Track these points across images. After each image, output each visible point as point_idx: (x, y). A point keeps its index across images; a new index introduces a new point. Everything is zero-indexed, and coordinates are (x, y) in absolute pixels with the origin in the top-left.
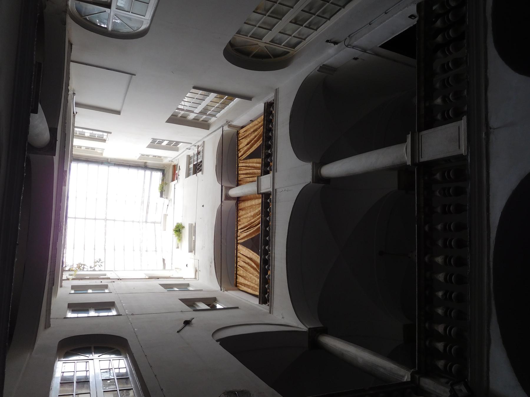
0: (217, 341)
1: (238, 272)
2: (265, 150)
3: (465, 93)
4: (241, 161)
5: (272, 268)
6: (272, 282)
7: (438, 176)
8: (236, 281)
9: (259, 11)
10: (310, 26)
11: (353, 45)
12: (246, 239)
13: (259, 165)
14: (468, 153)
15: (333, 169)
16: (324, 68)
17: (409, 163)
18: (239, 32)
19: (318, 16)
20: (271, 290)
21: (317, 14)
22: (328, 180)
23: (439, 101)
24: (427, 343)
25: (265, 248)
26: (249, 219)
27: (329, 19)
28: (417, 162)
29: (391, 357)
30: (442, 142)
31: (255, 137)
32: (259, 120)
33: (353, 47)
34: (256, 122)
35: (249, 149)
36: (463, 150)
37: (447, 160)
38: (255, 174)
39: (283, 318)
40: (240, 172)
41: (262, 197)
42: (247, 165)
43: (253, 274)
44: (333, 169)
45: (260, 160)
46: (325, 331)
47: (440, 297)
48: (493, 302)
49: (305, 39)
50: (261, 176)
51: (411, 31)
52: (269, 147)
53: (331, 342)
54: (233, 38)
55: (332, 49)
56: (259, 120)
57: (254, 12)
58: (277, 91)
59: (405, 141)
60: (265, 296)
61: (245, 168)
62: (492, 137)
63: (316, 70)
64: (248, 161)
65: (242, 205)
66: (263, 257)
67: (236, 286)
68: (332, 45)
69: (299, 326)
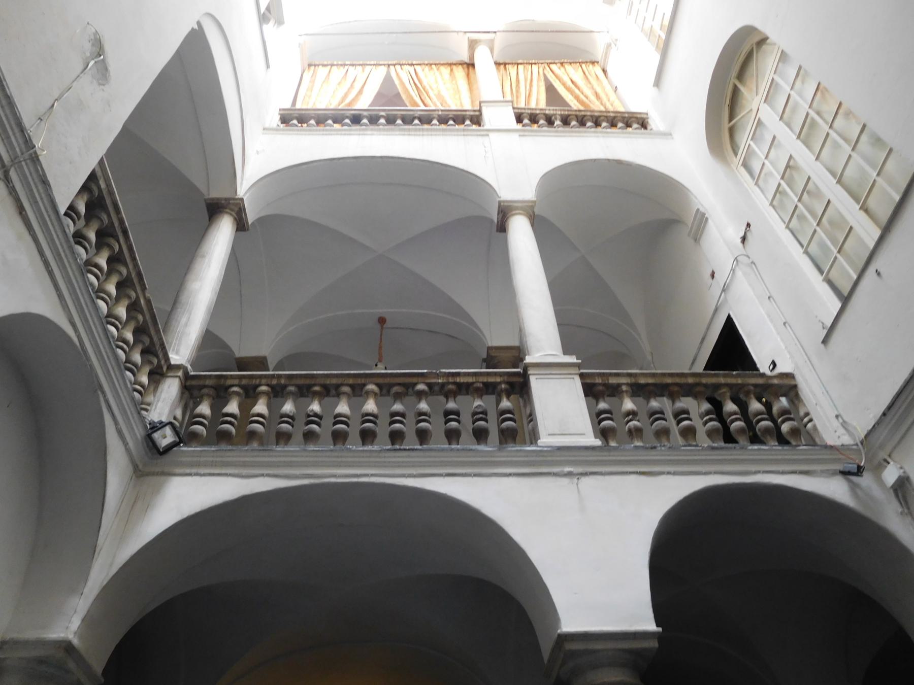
0: (199, 23)
1: (334, 68)
2: (561, 115)
5: (345, 130)
7: (505, 404)
12: (397, 82)
15: (521, 234)
16: (701, 220)
17: (528, 359)
19: (796, 206)
21: (800, 205)
22: (502, 227)
23: (628, 404)
24: (235, 389)
25: (382, 116)
30: (561, 409)
31: (587, 97)
33: (733, 270)
35: (564, 84)
36: (545, 440)
37: (531, 417)
38: (517, 97)
39: (258, 152)
41: (475, 111)
44: (521, 234)
45: (543, 104)
46: (241, 225)
47: (311, 408)
48: (306, 482)
49: (756, 184)
50: (514, 108)
52: (566, 121)
53: (223, 234)
58: (667, 135)
59: (566, 352)
62: (565, 481)
65: (460, 72)
66: (365, 113)
67: (310, 65)
68: (742, 234)
69: (244, 182)
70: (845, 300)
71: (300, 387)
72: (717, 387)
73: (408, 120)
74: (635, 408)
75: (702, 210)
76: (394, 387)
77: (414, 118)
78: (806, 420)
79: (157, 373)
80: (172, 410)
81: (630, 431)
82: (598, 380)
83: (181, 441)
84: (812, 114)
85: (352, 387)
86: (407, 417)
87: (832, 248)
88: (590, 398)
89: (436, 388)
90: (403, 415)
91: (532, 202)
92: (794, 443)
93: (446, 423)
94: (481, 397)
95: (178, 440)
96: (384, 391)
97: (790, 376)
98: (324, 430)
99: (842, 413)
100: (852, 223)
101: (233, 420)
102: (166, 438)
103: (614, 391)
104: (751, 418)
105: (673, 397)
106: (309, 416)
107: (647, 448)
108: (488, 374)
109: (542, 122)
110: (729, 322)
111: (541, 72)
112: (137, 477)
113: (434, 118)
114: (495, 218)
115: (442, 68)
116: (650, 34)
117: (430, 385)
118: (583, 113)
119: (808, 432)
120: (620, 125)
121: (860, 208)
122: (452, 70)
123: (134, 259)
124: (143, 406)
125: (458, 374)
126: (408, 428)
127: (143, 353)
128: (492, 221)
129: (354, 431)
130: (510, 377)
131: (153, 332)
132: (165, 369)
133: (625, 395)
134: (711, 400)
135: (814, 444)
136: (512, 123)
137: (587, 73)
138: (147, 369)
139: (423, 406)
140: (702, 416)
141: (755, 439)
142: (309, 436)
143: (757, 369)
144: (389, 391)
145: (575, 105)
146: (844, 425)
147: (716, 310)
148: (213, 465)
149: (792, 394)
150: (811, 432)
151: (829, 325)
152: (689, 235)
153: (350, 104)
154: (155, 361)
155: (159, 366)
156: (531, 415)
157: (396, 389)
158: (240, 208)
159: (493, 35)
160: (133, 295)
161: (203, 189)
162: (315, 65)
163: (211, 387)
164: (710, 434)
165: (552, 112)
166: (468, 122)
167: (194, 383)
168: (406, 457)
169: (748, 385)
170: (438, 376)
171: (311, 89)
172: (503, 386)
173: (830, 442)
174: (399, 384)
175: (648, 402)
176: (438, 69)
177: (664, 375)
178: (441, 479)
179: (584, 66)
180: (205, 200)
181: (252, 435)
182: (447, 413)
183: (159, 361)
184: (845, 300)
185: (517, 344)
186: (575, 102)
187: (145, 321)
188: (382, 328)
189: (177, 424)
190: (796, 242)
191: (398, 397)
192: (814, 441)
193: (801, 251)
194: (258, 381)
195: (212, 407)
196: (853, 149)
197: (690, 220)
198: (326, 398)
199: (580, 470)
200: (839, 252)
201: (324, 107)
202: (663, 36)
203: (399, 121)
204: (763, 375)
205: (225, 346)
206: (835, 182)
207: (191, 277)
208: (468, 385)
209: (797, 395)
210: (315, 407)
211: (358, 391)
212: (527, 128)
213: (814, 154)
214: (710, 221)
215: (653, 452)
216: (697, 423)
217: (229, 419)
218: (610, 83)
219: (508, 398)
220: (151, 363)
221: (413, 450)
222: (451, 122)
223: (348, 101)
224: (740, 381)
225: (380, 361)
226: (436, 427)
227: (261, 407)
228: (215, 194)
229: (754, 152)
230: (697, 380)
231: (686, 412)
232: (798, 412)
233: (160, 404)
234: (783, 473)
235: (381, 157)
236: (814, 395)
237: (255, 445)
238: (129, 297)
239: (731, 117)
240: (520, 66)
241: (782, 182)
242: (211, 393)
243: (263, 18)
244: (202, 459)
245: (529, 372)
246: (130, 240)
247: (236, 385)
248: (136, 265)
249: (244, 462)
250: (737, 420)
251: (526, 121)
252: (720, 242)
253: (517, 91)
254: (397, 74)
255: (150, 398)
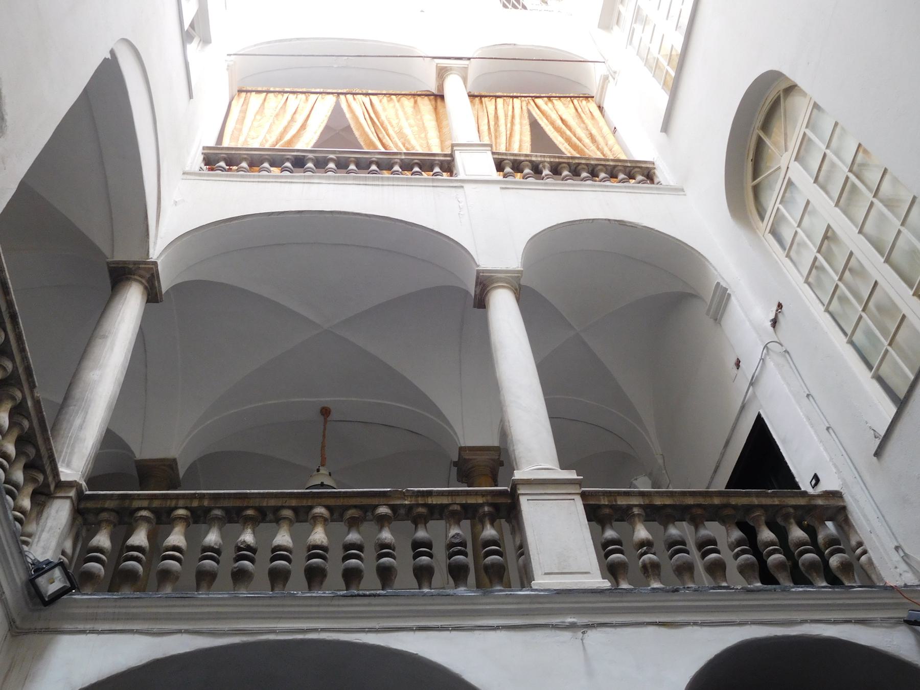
0: (112, 52)
1: (271, 95)
2: (550, 163)
3: (656, 585)
4: (524, 104)
5: (286, 177)
6: (254, 177)
7: (489, 532)
8: (251, 91)
9: (860, 155)
10: (817, 268)
11: (768, 360)
12: (348, 115)
13: (515, 150)
14: (536, 590)
15: (504, 310)
16: (723, 296)
17: (518, 475)
18: (816, 106)
19: (837, 286)
20: (237, 176)
21: (840, 284)
22: (481, 302)
23: (642, 533)
24: (144, 513)
25: (332, 160)
26: (394, 122)
27: (827, 310)
28: (519, 492)
29: (110, 439)
30: (559, 540)
31: (580, 140)
32: (616, 148)
33: (763, 360)
34: (611, 140)
35: (552, 123)
36: (541, 581)
37: (522, 550)
38: (496, 138)
39: (176, 203)
40: (500, 101)
41: (445, 155)
42: (517, 120)
43: (269, 132)
44: (504, 310)
45: (527, 150)
46: (153, 295)
47: (242, 538)
48: (236, 640)
49: (788, 256)
50: (493, 153)
51: (787, 479)
52: (556, 170)
53: (130, 307)
54: (804, 94)
55: (764, 316)
56: (616, 148)
57: (860, 145)
58: (678, 190)
59: (564, 466)
60: (219, 160)
61: (510, 113)
62: (566, 635)
63: (720, 280)
64: (526, 122)
65: (426, 105)
66: (311, 155)
67: (240, 91)
68: (772, 316)
69: (159, 241)
70: (901, 403)
71: (226, 510)
72: (749, 509)
73: (363, 165)
74: (650, 537)
75: (723, 284)
76: (349, 510)
77: (371, 163)
78: (859, 551)
79: (42, 493)
80: (60, 543)
81: (644, 567)
82: (604, 501)
83: (73, 587)
84: (852, 177)
85: (295, 510)
86: (365, 549)
87: (882, 339)
88: (594, 523)
89: (402, 511)
90: (360, 548)
91: (518, 272)
92: (847, 584)
93: (415, 557)
94: (458, 523)
95: (68, 585)
96: (336, 516)
97: (836, 495)
98: (259, 568)
99: (903, 544)
100: (905, 310)
101: (140, 555)
102: (53, 583)
103: (623, 515)
104: (792, 549)
105: (697, 523)
106: (239, 549)
107: (668, 591)
108: (468, 493)
109: (527, 171)
110: (760, 422)
111: (524, 108)
112: (13, 636)
113: (396, 163)
114: (472, 289)
115: (404, 99)
116: (655, 68)
117: (393, 508)
118: (577, 161)
119: (862, 567)
120: (621, 176)
121: (914, 295)
122: (416, 102)
123: (22, 350)
124: (23, 538)
125: (430, 493)
126: (367, 564)
127: (26, 468)
128: (467, 293)
129: (297, 569)
130: (488, 492)
131: (40, 441)
132: (52, 487)
133: (637, 519)
134: (743, 526)
135: (873, 586)
136: (491, 171)
137: (580, 110)
138: (29, 489)
139: (386, 535)
140: (732, 547)
141: (799, 578)
142: (240, 576)
143: (799, 488)
144: (341, 516)
145: (567, 150)
146: (906, 558)
147: (743, 407)
148: (115, 618)
149: (840, 518)
150: (866, 567)
151: (882, 433)
152: (707, 314)
153: (290, 142)
154: (41, 478)
155: (46, 485)
156: (521, 547)
157: (351, 513)
158: (153, 275)
159: (467, 62)
160: (19, 395)
161: (106, 250)
162: (247, 91)
163: (112, 510)
164: (743, 570)
165: (539, 159)
166: (437, 169)
167: (90, 505)
168: (365, 605)
169: (787, 506)
170: (404, 495)
171: (241, 120)
172: (486, 509)
173: (891, 582)
174: (355, 507)
175: (666, 529)
176: (399, 101)
177: (684, 494)
178: (411, 634)
179: (575, 101)
180: (108, 263)
181: (165, 576)
182: (416, 544)
183: (46, 478)
184: (901, 403)
185: (496, 444)
186: (566, 145)
187: (31, 427)
188: (326, 422)
189: (66, 560)
190: (837, 329)
191: (353, 523)
192: (869, 578)
193: (845, 340)
194: (173, 504)
195: (113, 539)
196: (903, 224)
197: (708, 295)
198: (262, 525)
199: (585, 620)
200: (890, 344)
201: (257, 146)
202: (673, 74)
203: (352, 167)
204: (805, 493)
205: (126, 447)
206: (883, 260)
207: (88, 363)
208: (443, 507)
209: (847, 520)
210: (248, 537)
211: (302, 514)
212: (510, 179)
213: (857, 227)
214: (733, 298)
215: (675, 597)
216: (726, 555)
217: (135, 553)
218: (608, 123)
219: (492, 524)
220: (35, 480)
221: (374, 595)
222: (416, 169)
223: (287, 137)
224: (776, 501)
225: (323, 465)
226: (403, 563)
227: (177, 538)
228: (121, 255)
229: (783, 218)
230: (725, 500)
231: (713, 542)
232: (849, 540)
233: (45, 536)
234: (836, 622)
235: (331, 212)
236: (868, 520)
237: (168, 590)
238: (13, 398)
239: (756, 173)
240: (499, 100)
241: (819, 256)
242: (112, 518)
243: (187, 37)
244: (100, 611)
245: (519, 492)
246: (19, 328)
247: (145, 509)
248: (25, 358)
249: (156, 613)
250: (774, 552)
251: (508, 169)
252: (746, 323)
253: (496, 130)
254: (349, 106)
255: (31, 528)
